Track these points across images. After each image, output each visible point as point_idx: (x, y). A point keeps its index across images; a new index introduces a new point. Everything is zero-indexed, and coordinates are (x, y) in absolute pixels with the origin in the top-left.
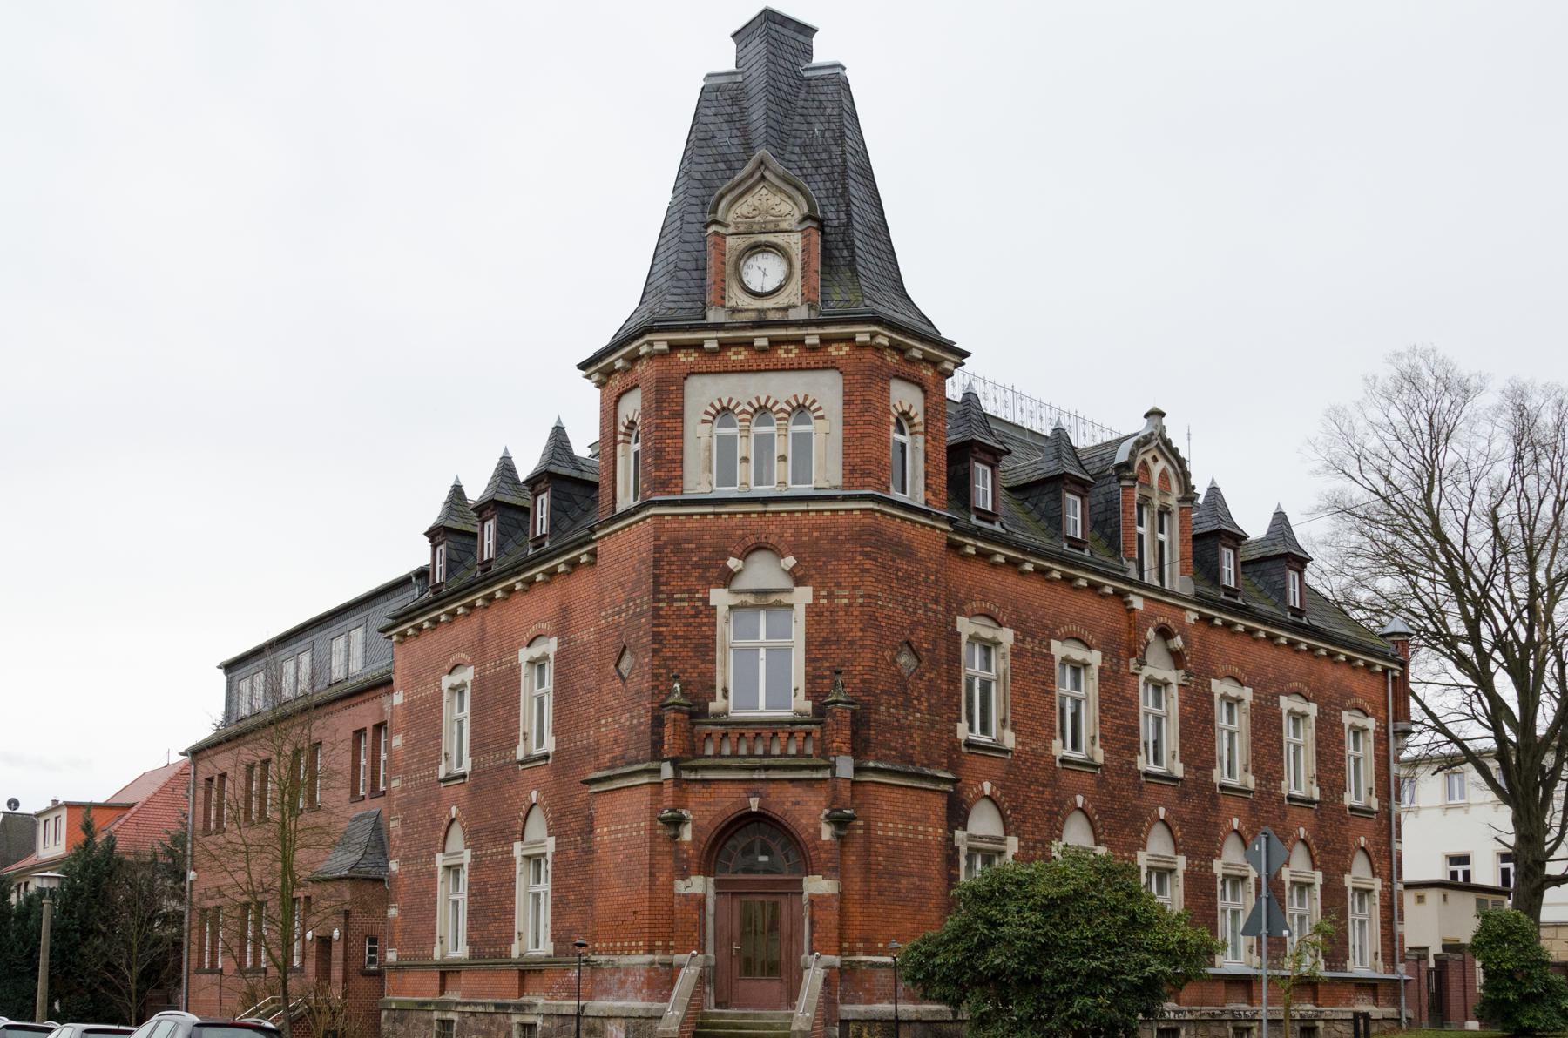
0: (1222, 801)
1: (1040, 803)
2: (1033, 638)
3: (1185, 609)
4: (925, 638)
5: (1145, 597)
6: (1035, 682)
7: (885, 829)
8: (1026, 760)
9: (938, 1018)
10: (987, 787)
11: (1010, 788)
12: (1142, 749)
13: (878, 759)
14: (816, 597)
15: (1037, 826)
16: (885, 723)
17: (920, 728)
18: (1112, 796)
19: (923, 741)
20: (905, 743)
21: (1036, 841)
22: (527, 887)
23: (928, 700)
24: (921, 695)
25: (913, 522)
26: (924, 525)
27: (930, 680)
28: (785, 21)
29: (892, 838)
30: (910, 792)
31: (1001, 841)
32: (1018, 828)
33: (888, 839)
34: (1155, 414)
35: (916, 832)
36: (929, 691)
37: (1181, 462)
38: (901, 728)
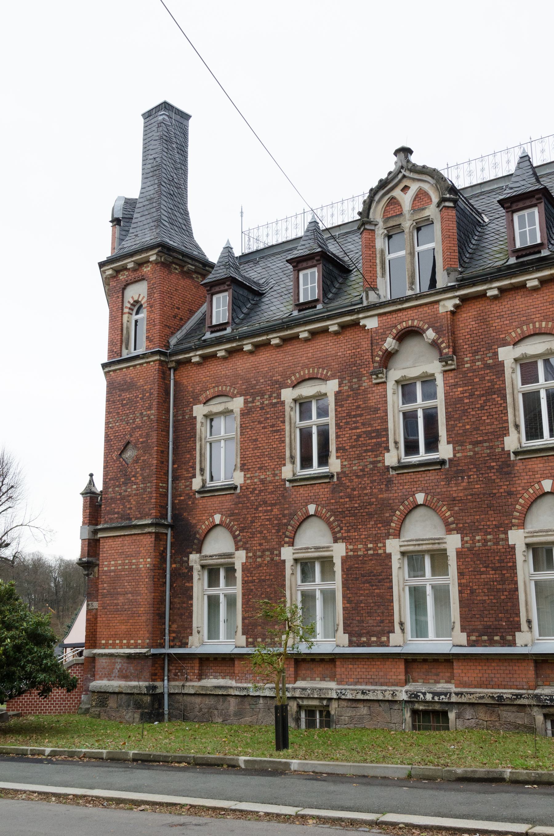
0: (519, 466)
1: (268, 520)
2: (262, 396)
3: (437, 302)
4: (141, 436)
5: (379, 315)
6: (264, 428)
7: (108, 566)
8: (255, 489)
9: (136, 691)
10: (217, 518)
11: (239, 514)
12: (391, 445)
13: (106, 522)
14: (340, 384)
15: (265, 538)
16: (112, 498)
17: (136, 495)
18: (350, 496)
19: (138, 503)
20: (125, 507)
21: (264, 551)
22: (405, 581)
23: (142, 475)
24: (137, 473)
25: (135, 366)
26: (141, 364)
27: (144, 461)
28: (169, 104)
29: (114, 571)
30: (127, 538)
31: (230, 555)
32: (245, 543)
33: (110, 571)
34: (404, 152)
35: (131, 564)
36: (142, 469)
37: (373, 192)
38: (123, 498)
